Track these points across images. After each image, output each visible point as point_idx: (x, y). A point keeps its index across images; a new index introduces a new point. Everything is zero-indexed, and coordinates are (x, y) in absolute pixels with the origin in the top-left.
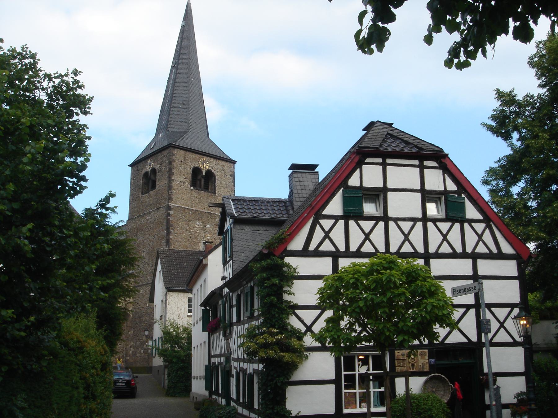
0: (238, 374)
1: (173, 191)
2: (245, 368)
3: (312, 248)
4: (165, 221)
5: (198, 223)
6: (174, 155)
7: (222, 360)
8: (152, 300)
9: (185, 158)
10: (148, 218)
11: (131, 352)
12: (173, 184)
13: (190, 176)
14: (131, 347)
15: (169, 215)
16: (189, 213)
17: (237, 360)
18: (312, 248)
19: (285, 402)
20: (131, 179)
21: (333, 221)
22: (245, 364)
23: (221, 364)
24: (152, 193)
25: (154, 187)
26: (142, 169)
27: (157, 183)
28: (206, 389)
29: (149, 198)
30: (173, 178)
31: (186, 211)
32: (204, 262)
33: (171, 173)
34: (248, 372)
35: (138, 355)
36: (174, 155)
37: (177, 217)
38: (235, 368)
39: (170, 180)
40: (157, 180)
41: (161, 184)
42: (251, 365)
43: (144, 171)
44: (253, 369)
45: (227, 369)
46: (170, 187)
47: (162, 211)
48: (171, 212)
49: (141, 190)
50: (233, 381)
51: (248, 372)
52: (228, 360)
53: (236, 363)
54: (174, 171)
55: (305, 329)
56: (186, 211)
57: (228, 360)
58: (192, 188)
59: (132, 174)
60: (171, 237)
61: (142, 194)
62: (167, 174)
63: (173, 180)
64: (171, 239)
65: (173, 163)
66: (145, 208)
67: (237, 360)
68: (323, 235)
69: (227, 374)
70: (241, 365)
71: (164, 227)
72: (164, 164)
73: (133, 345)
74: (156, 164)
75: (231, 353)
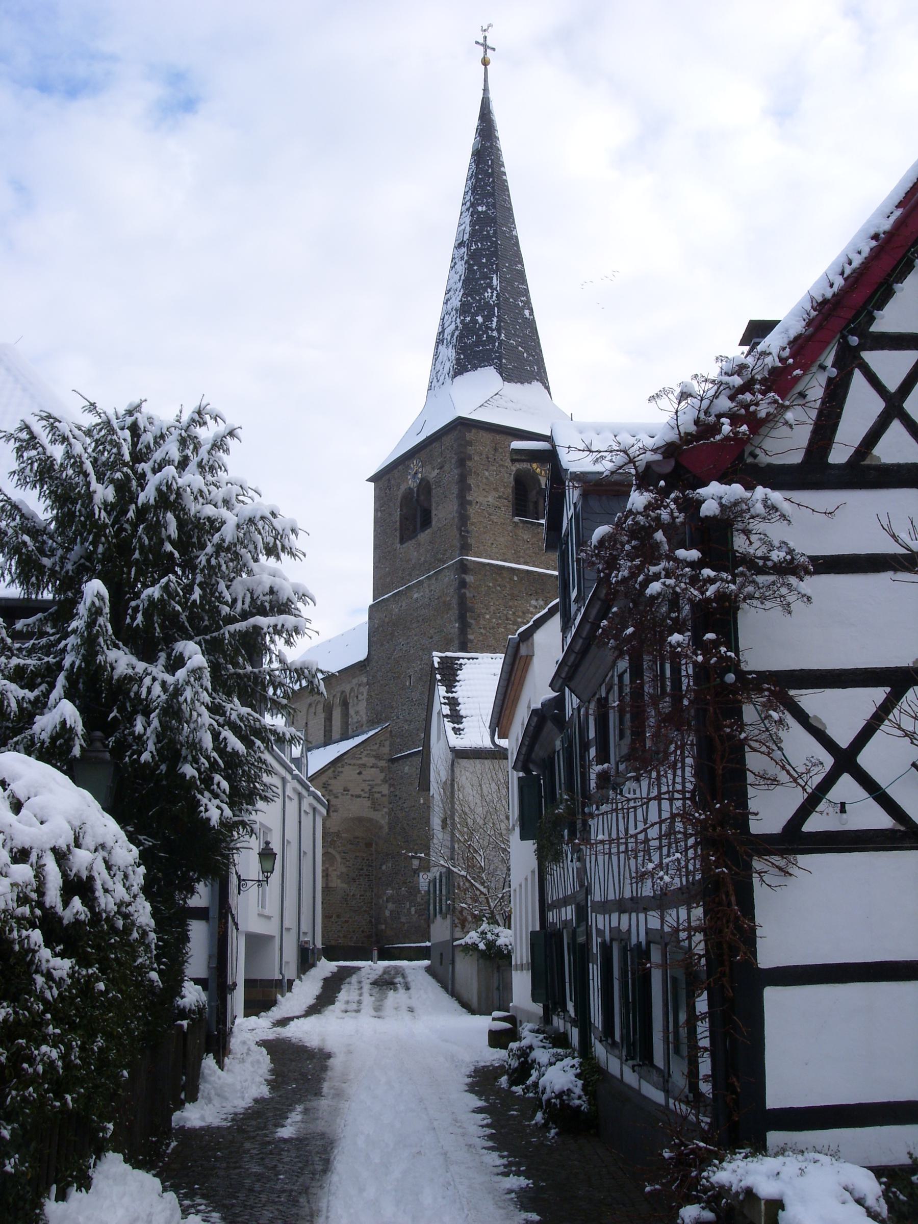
0: (606, 949)
1: (471, 528)
2: (624, 927)
3: (839, 455)
4: (454, 602)
5: (533, 602)
6: (470, 443)
7: (568, 913)
8: (425, 785)
9: (496, 450)
10: (416, 596)
11: (387, 913)
12: (472, 511)
13: (510, 491)
14: (387, 901)
15: (463, 584)
16: (511, 579)
17: (605, 907)
18: (839, 455)
19: (140, 1169)
20: (376, 511)
21: (879, 694)
22: (625, 917)
23: (566, 923)
24: (423, 537)
25: (426, 522)
26: (398, 486)
27: (434, 512)
28: (535, 999)
29: (413, 551)
30: (469, 498)
31: (505, 574)
32: (523, 651)
33: (464, 487)
34: (634, 941)
35: (403, 920)
36: (470, 443)
37: (484, 589)
38: (600, 933)
39: (463, 503)
40: (433, 507)
41: (444, 512)
42: (642, 916)
43: (403, 488)
44: (648, 931)
45: (581, 939)
46: (463, 519)
47: (450, 578)
48: (469, 578)
49: (397, 533)
50: (595, 972)
51: (634, 941)
52: (582, 913)
53: (600, 918)
54: (471, 481)
55: (797, 458)
56: (505, 574)
57: (582, 913)
58: (517, 519)
59: (378, 498)
60: (471, 637)
61: (402, 541)
62: (455, 490)
63: (470, 503)
64: (471, 641)
65: (469, 463)
66: (410, 575)
67: (605, 907)
68: (879, 405)
69: (582, 954)
70: (614, 924)
71: (454, 612)
72: (447, 467)
73: (392, 895)
74: (428, 468)
75: (588, 891)
